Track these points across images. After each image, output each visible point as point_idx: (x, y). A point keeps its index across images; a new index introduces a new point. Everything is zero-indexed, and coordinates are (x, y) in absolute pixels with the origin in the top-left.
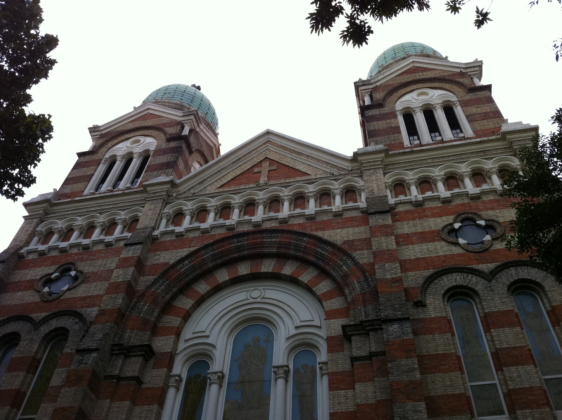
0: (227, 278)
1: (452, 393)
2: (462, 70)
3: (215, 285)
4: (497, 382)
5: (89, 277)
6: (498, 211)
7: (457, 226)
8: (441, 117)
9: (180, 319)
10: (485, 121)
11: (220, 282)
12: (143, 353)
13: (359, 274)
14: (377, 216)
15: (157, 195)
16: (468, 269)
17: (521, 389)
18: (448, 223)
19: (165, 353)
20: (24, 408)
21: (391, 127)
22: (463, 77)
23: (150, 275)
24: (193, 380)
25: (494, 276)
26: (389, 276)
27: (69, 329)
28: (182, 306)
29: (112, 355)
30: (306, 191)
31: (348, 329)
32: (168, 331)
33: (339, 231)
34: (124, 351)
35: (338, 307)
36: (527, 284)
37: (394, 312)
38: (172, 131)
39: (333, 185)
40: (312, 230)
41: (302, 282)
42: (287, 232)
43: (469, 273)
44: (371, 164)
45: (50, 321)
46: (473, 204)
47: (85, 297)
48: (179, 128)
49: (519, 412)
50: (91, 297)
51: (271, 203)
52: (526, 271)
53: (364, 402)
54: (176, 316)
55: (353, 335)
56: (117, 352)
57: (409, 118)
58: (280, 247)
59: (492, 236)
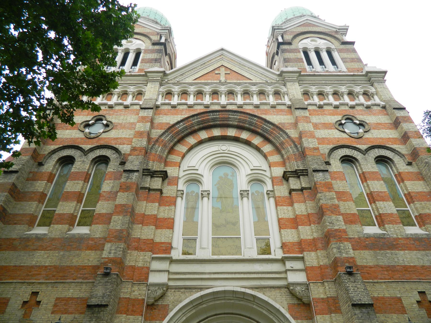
0: (207, 137)
1: (349, 212)
2: (337, 30)
3: (199, 140)
4: (370, 208)
5: (117, 126)
6: (365, 116)
7: (343, 122)
8: (325, 56)
10: (353, 63)
11: (203, 138)
12: (162, 175)
13: (290, 143)
14: (300, 111)
15: (155, 79)
16: (353, 147)
17: (387, 214)
18: (338, 120)
20: (404, 201)
21: (298, 58)
22: (337, 34)
23: (158, 129)
24: (190, 194)
25: (367, 152)
26: (311, 146)
27: (110, 157)
28: (180, 150)
29: (143, 175)
30: (236, 90)
31: (288, 173)
33: (275, 116)
35: (277, 161)
36: (383, 159)
37: (319, 167)
38: (155, 38)
39: (205, 88)
40: (258, 114)
41: (253, 144)
42: (241, 112)
43: (353, 149)
44: (291, 79)
45: (95, 151)
46: (351, 110)
47: (117, 138)
48: (159, 37)
49: (386, 226)
51: (197, 94)
52: (384, 151)
53: (300, 214)
54: (178, 156)
55: (290, 177)
56: (146, 174)
57: (306, 54)
58: (239, 122)
59: (363, 130)
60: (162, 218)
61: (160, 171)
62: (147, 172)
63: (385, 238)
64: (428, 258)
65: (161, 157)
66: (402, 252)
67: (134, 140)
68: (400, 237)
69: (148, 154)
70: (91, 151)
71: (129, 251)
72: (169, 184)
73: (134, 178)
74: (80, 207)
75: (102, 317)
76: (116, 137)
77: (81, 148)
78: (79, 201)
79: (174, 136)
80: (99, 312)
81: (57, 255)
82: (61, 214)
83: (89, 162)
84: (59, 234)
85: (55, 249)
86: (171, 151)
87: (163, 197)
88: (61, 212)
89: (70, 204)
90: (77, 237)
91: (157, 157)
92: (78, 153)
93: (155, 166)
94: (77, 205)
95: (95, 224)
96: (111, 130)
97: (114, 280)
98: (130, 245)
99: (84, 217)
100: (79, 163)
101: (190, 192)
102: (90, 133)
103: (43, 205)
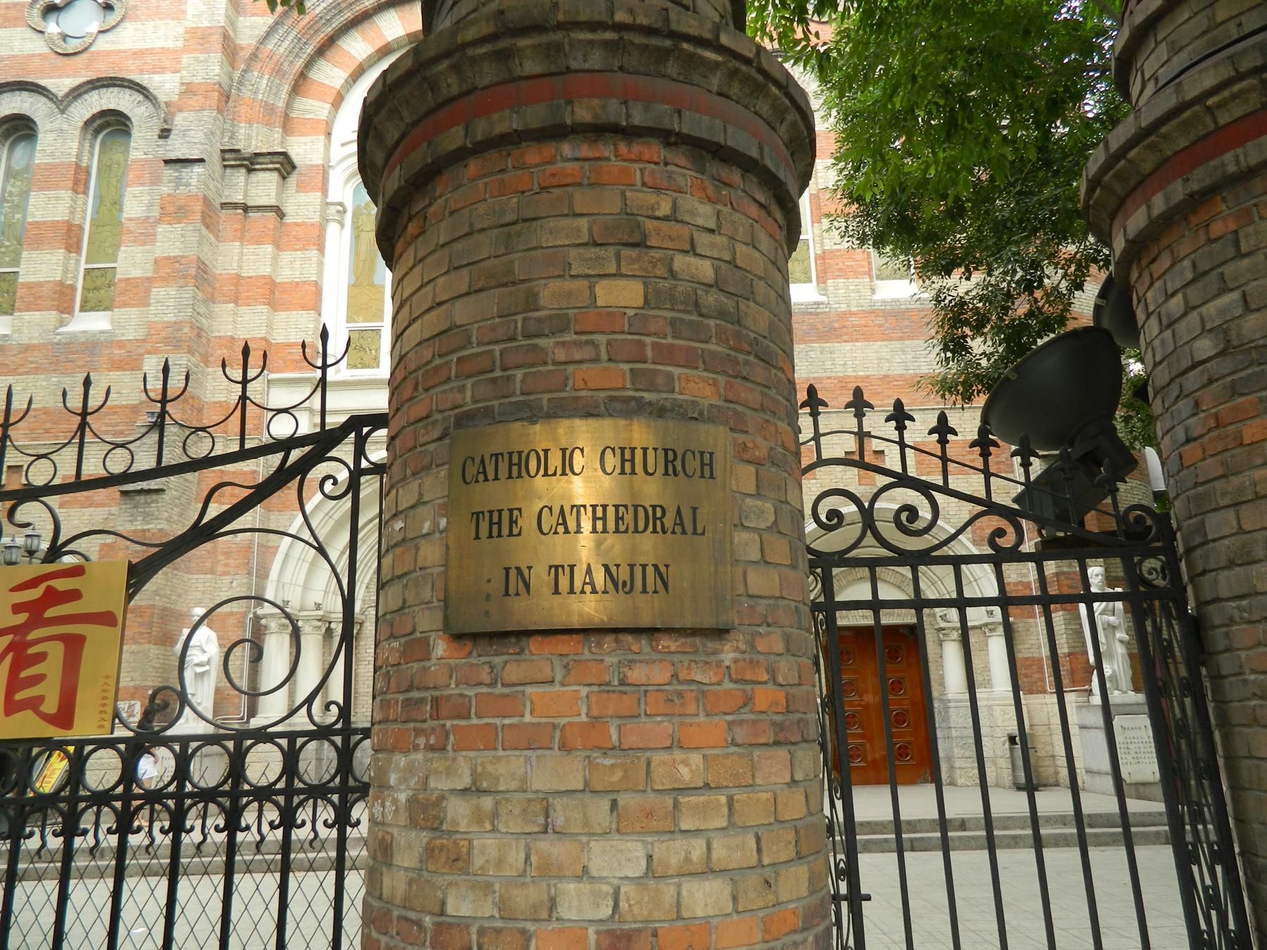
3: (380, 44)
9: (328, 106)
11: (390, 39)
12: (278, 166)
19: (312, 165)
23: (257, 15)
27: (130, 115)
28: (326, 82)
29: (225, 166)
32: (311, 127)
34: (245, 163)
45: (86, 96)
50: (151, 51)
60: (287, 283)
61: (270, 154)
62: (235, 159)
63: (817, 314)
64: (903, 357)
65: (269, 109)
66: (847, 346)
67: (185, 59)
68: (854, 309)
69: (231, 104)
70: (76, 98)
71: (210, 370)
72: (301, 188)
73: (194, 182)
74: (78, 261)
75: (156, 513)
76: (139, 46)
77: (44, 89)
78: (72, 245)
79: (303, 36)
80: (147, 504)
81: (44, 383)
82: (33, 283)
83: (77, 133)
84: (37, 335)
85: (37, 370)
86: (300, 83)
87: (287, 225)
88: (32, 279)
89: (49, 255)
90: (83, 340)
91: (257, 109)
92: (40, 104)
93: (255, 139)
94: (67, 259)
95: (120, 307)
96: (123, 25)
97: (173, 438)
98: (212, 356)
99: (95, 289)
100: (51, 136)
101: (363, 205)
102: (65, 37)
103: (88, 196)
